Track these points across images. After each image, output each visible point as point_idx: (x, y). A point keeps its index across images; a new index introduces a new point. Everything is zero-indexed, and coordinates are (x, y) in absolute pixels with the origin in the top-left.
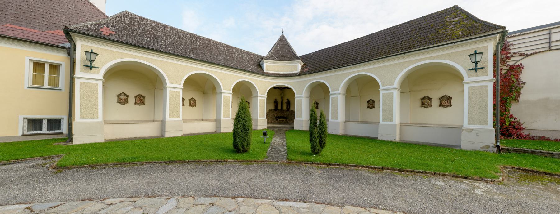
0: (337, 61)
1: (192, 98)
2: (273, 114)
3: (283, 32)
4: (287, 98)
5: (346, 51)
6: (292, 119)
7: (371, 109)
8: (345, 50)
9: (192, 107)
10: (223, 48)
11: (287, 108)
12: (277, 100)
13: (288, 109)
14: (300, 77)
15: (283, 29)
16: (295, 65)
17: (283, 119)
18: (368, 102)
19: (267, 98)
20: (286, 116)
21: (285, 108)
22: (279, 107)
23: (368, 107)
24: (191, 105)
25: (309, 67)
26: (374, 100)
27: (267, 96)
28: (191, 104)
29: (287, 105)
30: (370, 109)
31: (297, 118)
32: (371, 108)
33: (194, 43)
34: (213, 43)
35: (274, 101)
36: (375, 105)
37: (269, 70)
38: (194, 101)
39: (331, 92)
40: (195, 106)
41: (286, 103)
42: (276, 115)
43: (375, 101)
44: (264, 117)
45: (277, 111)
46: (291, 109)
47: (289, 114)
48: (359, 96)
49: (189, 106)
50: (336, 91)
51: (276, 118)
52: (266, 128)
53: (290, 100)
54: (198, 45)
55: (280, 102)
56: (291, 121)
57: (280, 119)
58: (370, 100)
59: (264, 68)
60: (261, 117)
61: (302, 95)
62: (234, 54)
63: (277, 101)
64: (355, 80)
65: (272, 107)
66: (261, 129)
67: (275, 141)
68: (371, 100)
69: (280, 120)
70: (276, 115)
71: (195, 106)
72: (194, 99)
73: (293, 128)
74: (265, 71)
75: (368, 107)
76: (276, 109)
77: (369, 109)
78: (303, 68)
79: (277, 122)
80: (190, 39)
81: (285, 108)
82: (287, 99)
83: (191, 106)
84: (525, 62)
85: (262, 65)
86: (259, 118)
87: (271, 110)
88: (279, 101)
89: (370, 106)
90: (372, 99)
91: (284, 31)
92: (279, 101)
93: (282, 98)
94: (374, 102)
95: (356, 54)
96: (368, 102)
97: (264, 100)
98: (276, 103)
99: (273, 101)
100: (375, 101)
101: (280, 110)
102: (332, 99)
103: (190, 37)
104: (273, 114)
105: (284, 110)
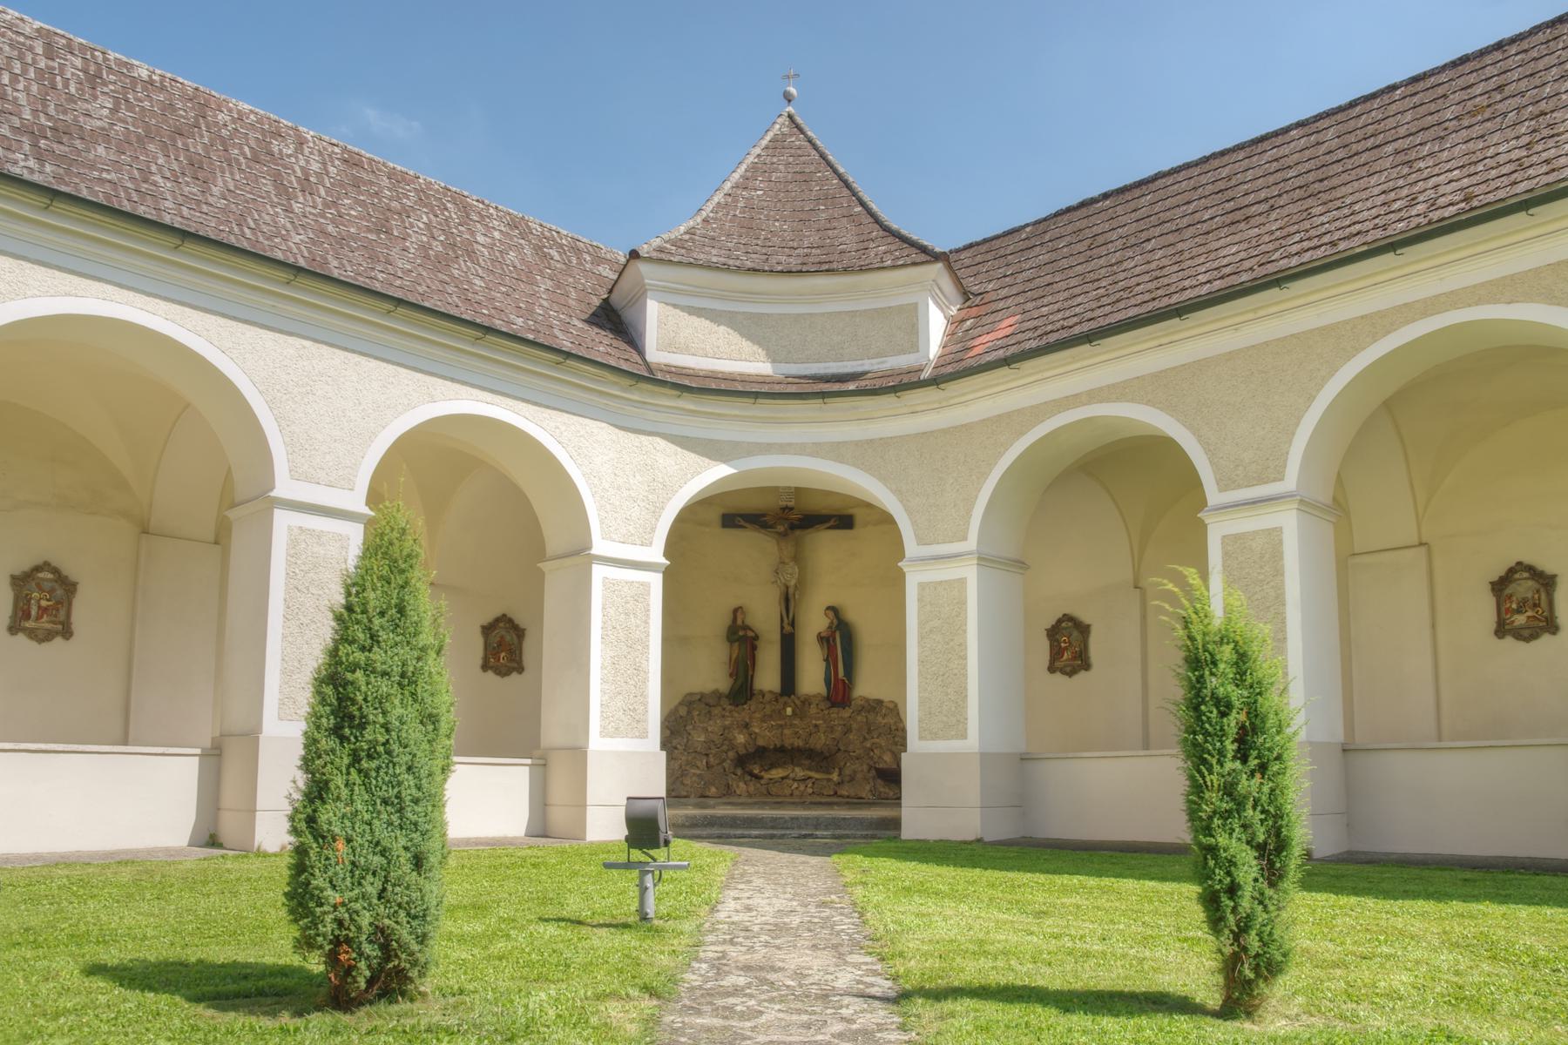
0: (1245, 246)
1: (37, 569)
4: (830, 602)
5: (1311, 177)
7: (1528, 639)
8: (1292, 173)
9: (41, 641)
10: (315, 167)
11: (827, 681)
12: (749, 621)
13: (839, 692)
18: (1500, 586)
20: (820, 741)
21: (812, 676)
22: (768, 678)
23: (1502, 630)
24: (29, 624)
25: (1012, 320)
26: (1547, 565)
27: (667, 554)
28: (27, 615)
29: (830, 660)
30: (1522, 644)
31: (927, 734)
32: (1528, 634)
33: (71, 98)
34: (234, 121)
36: (1557, 613)
38: (59, 592)
39: (1214, 496)
40: (67, 633)
43: (1553, 577)
45: (753, 704)
46: (867, 686)
47: (848, 731)
48: (1421, 544)
49: (13, 629)
50: (1262, 480)
51: (742, 761)
54: (105, 112)
58: (1511, 571)
59: (642, 335)
60: (617, 734)
62: (405, 212)
63: (746, 628)
64: (1384, 403)
65: (711, 675)
67: (748, 909)
68: (1520, 566)
69: (777, 773)
70: (741, 738)
71: (67, 633)
72: (55, 571)
73: (895, 824)
74: (656, 353)
75: (1502, 630)
76: (742, 689)
77: (1509, 640)
78: (958, 334)
80: (42, 65)
81: (812, 676)
82: (834, 610)
83: (32, 634)
85: (628, 315)
86: (597, 743)
87: (702, 695)
88: (765, 618)
89: (1520, 620)
90: (1528, 559)
92: (765, 618)
93: (787, 601)
94: (1547, 582)
95: (1401, 182)
96: (1500, 586)
98: (741, 638)
99: (714, 623)
100: (1553, 577)
101: (777, 697)
102: (1226, 555)
103: (39, 50)
105: (807, 701)
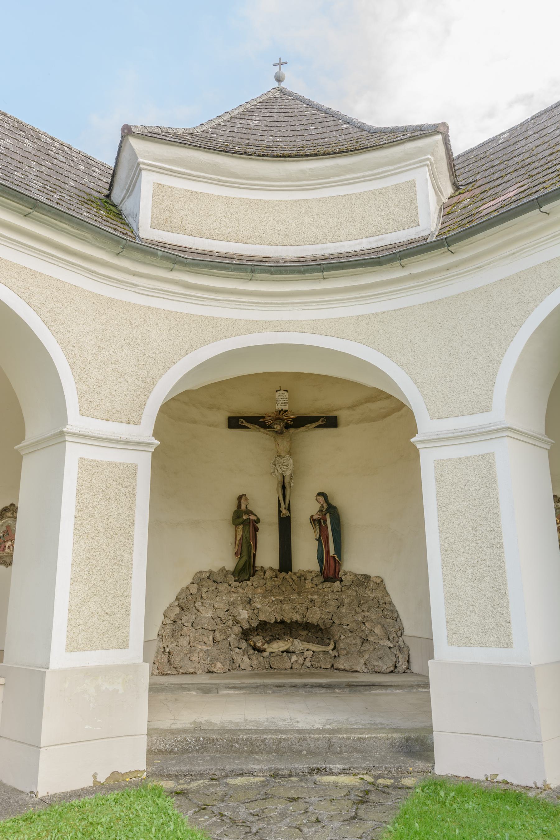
2: (221, 603)
3: (279, 79)
6: (364, 641)
14: (450, 260)
15: (280, 64)
16: (397, 187)
17: (298, 645)
19: (155, 455)
27: (156, 434)
29: (322, 540)
35: (235, 508)
37: (182, 230)
41: (313, 521)
42: (244, 614)
44: (124, 644)
51: (246, 634)
52: (141, 764)
53: (338, 501)
55: (276, 520)
56: (360, 653)
57: (275, 638)
59: (136, 216)
61: (488, 409)
63: (250, 512)
66: (88, 783)
69: (278, 646)
70: (244, 614)
79: (254, 673)
84: (156, 638)
85: (127, 207)
91: (285, 71)
97: (133, 468)
104: (221, 603)
105: (302, 577)
